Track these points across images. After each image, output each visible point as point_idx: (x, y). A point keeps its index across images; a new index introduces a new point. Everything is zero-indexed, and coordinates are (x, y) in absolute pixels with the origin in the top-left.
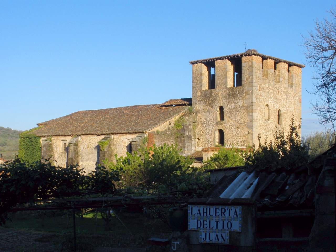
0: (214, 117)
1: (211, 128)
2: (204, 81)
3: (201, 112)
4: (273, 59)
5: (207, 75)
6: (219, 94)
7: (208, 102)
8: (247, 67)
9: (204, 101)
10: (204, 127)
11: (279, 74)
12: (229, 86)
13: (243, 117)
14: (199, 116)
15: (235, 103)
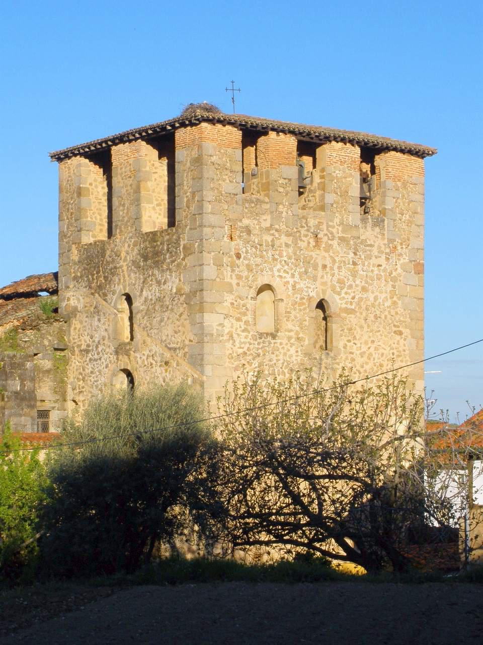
0: (110, 332)
1: (104, 365)
2: (89, 213)
3: (78, 314)
4: (292, 132)
5: (101, 193)
6: (122, 255)
7: (95, 281)
8: (188, 164)
9: (86, 279)
10: (87, 364)
11: (321, 182)
12: (146, 228)
13: (180, 328)
14: (75, 329)
15: (159, 283)
